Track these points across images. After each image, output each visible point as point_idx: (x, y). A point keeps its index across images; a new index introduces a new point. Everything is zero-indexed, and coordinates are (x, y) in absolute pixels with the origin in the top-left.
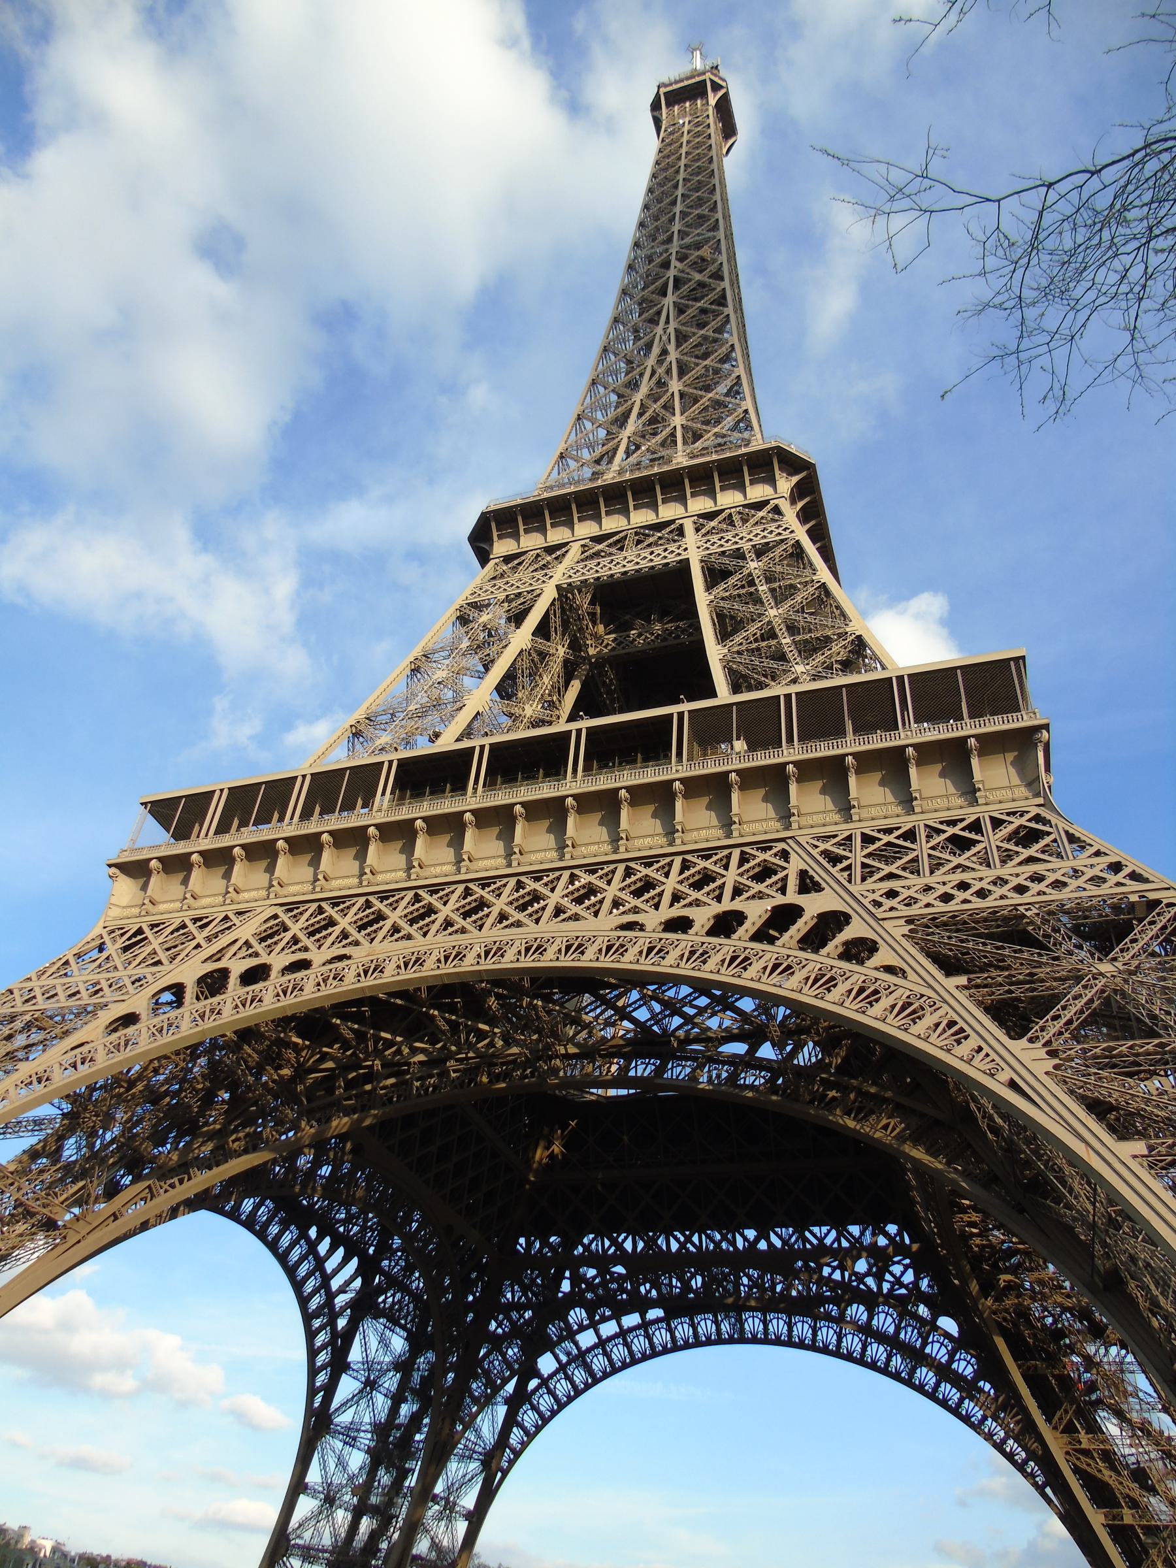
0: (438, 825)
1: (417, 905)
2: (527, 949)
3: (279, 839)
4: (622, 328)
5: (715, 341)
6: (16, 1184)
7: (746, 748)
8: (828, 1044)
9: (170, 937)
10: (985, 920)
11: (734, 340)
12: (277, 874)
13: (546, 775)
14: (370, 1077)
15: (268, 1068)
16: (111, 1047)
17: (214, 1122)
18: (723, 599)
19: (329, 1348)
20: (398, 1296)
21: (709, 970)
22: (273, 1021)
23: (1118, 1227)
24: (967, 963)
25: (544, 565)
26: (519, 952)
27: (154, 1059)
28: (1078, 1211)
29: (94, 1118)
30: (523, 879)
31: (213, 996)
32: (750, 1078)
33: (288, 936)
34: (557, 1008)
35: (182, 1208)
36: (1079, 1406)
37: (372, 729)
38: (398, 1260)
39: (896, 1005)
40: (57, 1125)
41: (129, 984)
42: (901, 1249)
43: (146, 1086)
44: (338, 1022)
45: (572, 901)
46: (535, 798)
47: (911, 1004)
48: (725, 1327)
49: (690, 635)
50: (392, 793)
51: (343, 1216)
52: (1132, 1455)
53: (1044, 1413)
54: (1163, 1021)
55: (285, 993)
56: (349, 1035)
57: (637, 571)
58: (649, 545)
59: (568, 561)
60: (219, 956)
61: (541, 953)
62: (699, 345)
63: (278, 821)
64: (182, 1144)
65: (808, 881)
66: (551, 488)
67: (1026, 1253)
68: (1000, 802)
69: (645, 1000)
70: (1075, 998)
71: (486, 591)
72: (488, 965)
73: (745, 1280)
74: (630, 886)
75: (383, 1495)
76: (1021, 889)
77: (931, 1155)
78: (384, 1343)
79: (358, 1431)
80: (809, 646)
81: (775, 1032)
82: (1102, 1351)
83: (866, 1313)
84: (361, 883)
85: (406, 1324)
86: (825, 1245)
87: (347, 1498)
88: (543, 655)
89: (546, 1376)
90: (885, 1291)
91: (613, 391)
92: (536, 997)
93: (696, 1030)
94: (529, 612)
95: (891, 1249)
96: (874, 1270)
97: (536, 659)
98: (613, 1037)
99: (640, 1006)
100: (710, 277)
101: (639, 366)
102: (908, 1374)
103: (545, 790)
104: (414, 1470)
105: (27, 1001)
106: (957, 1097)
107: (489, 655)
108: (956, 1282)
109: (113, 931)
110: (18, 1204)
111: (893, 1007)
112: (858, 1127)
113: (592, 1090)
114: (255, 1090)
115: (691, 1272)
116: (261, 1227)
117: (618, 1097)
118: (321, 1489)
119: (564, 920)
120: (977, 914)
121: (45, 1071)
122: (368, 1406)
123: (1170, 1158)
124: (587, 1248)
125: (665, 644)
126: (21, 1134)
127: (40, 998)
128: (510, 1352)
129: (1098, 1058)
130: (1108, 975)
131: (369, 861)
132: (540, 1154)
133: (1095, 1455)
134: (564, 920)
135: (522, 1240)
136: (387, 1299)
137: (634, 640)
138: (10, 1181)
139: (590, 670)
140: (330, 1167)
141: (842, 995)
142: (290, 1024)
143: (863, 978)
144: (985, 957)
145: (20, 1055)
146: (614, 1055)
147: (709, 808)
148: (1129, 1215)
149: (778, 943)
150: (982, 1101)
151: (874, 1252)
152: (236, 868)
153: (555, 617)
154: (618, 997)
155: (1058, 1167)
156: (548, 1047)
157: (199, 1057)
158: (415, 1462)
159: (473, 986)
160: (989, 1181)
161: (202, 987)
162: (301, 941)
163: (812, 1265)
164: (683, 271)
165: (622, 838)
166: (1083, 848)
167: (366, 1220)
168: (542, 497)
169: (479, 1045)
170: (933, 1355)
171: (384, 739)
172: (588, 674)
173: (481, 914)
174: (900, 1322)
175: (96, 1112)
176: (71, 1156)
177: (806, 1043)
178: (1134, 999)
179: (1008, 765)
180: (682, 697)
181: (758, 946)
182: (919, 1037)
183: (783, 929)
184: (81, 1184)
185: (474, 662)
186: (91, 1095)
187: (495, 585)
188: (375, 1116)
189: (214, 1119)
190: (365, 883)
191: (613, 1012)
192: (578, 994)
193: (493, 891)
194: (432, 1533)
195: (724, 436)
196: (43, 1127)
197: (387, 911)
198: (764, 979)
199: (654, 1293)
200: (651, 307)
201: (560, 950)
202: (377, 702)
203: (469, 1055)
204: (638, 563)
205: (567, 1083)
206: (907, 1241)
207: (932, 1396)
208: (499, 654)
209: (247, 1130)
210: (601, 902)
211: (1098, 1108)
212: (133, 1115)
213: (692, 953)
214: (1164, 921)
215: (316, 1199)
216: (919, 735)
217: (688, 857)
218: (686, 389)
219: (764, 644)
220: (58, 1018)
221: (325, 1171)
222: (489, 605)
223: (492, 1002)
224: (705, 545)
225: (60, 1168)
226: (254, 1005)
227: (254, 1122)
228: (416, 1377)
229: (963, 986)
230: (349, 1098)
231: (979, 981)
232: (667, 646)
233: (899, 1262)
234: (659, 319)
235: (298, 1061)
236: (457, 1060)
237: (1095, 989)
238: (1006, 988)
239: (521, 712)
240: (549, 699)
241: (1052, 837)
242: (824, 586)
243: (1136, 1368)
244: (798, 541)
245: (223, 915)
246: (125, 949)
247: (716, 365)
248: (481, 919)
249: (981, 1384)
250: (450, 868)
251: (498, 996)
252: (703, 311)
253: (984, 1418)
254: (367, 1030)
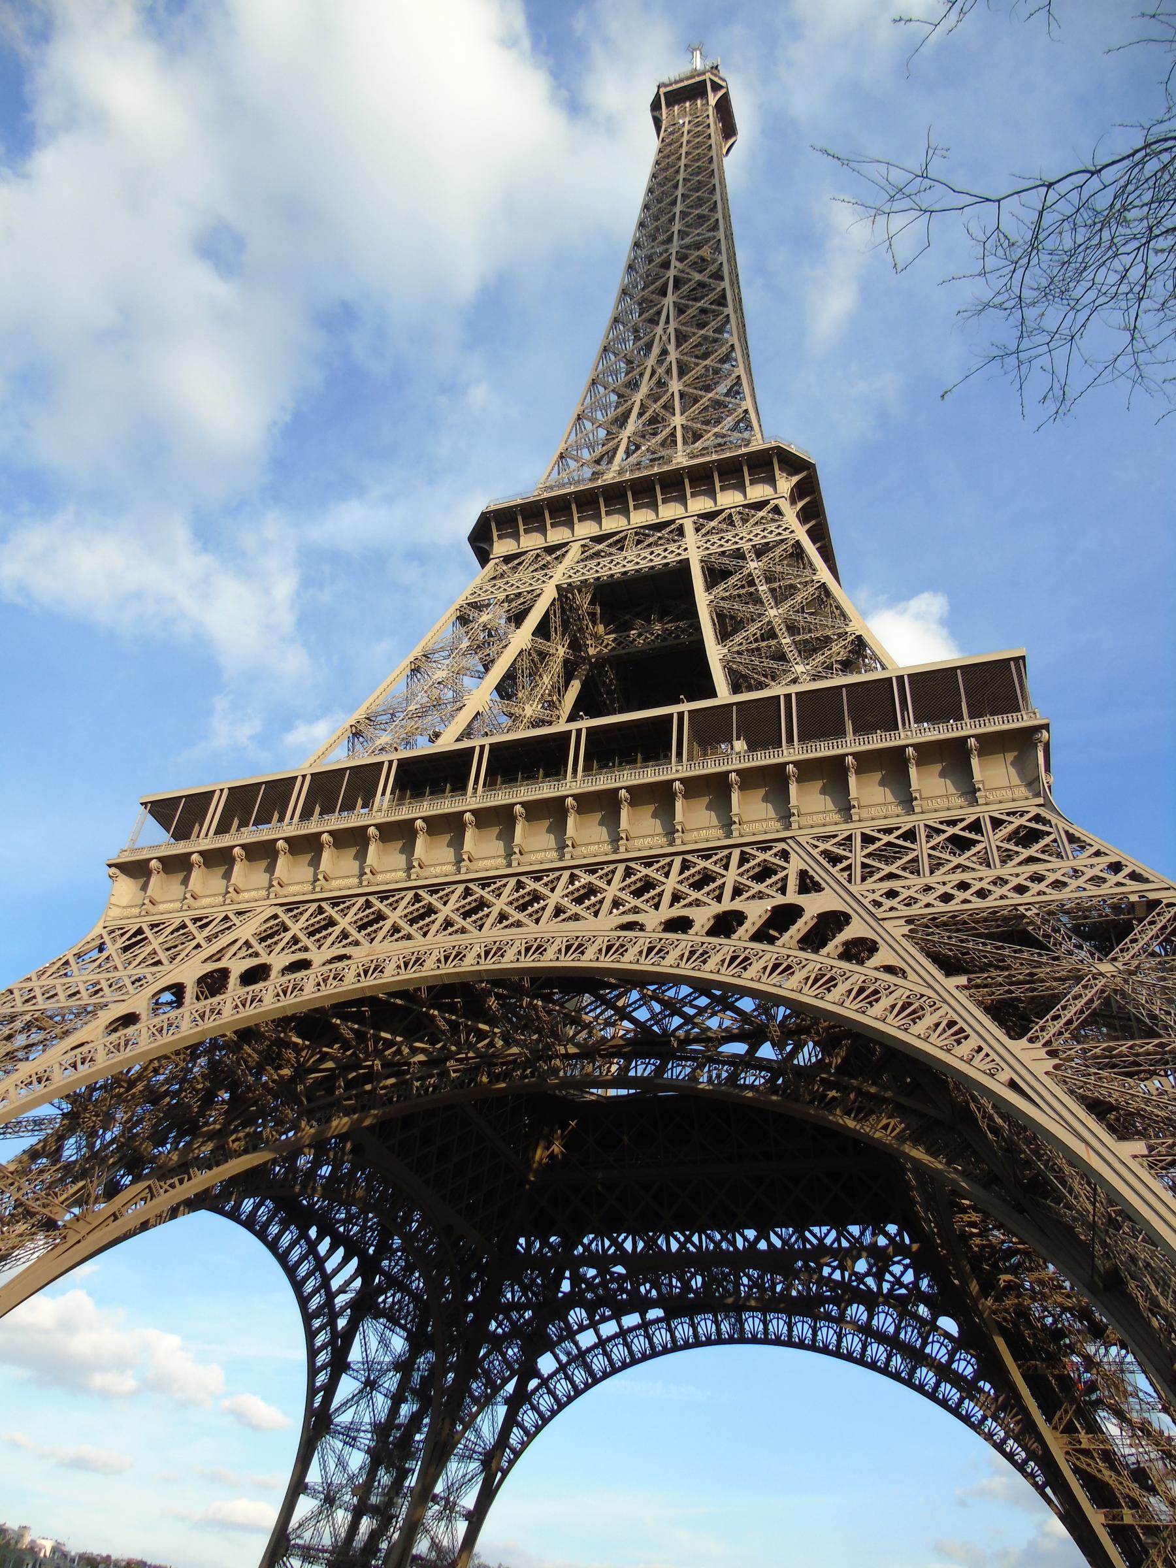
0: (438, 825)
1: (417, 905)
2: (527, 949)
3: (279, 839)
4: (622, 328)
5: (715, 341)
6: (16, 1184)
7: (746, 748)
8: (828, 1044)
9: (170, 937)
10: (985, 920)
11: (734, 340)
12: (277, 874)
13: (546, 775)
14: (370, 1077)
15: (268, 1068)
16: (111, 1047)
17: (214, 1122)
18: (723, 599)
19: (329, 1348)
20: (398, 1296)
21: (709, 970)
22: (273, 1021)
23: (1118, 1227)
24: (967, 963)
25: (544, 565)
26: (519, 952)
27: (154, 1059)
28: (1078, 1211)
29: (94, 1118)
30: (523, 879)
31: (213, 996)
32: (750, 1078)
33: (288, 936)
34: (557, 1008)
35: (182, 1208)
36: (1079, 1406)
37: (372, 729)
38: (398, 1260)
39: (896, 1005)
40: (57, 1125)
41: (129, 984)
42: (901, 1249)
43: (146, 1086)
44: (338, 1022)
45: (572, 901)
46: (535, 798)
47: (911, 1004)
48: (725, 1327)
49: (690, 635)
50: (392, 793)
51: (343, 1216)
52: (1132, 1455)
53: (1044, 1413)
54: (1163, 1021)
55: (285, 993)
56: (349, 1035)
57: (637, 571)
58: (649, 545)
59: (568, 561)
60: (219, 956)
61: (541, 953)
62: (699, 345)
63: (278, 821)
64: (182, 1144)
65: (808, 881)
66: (551, 488)
67: (1026, 1253)
68: (1000, 802)
69: (645, 1000)
70: (1075, 998)
71: (486, 591)
72: (488, 965)
73: (745, 1280)
74: (630, 886)
75: (383, 1495)
76: (1021, 889)
77: (931, 1155)
78: (384, 1343)
79: (358, 1431)
80: (809, 646)
81: (775, 1032)
82: (1102, 1351)
83: (866, 1313)
84: (361, 883)
85: (406, 1324)
86: (825, 1245)
87: (347, 1498)
88: (543, 655)
89: (546, 1376)
90: (885, 1291)
91: (613, 391)
92: (536, 997)
93: (696, 1030)
94: (529, 612)
95: (891, 1249)
96: (874, 1270)
97: (536, 659)
98: (613, 1037)
99: (640, 1006)
100: (710, 277)
101: (639, 366)
102: (908, 1374)
103: (545, 790)
104: (414, 1470)
105: (27, 1001)
106: (957, 1097)
107: (489, 655)
108: (956, 1282)
109: (113, 931)
111: (893, 1007)
112: (858, 1127)
113: (592, 1090)
114: (255, 1090)
115: (691, 1272)
116: (261, 1227)
117: (618, 1097)
118: (321, 1489)
119: (564, 920)
120: (977, 914)
121: (45, 1071)
122: (368, 1406)
123: (1170, 1158)
124: (587, 1248)
125: (665, 644)
126: (21, 1134)
127: (40, 998)
128: (510, 1352)
129: (1098, 1058)
130: (1108, 975)
131: (369, 861)
132: (540, 1154)
133: (1095, 1455)
134: (564, 920)
135: (522, 1240)
136: (387, 1299)
137: (634, 640)
138: (10, 1181)
139: (590, 670)
140: (330, 1167)
141: (842, 995)
142: (290, 1024)
143: (863, 978)
144: (985, 957)
145: (20, 1055)
146: (614, 1055)
147: (709, 808)
148: (1129, 1215)
149: (778, 943)
150: (982, 1101)
151: (874, 1252)
152: (236, 868)
153: (555, 617)
154: (618, 997)
155: (1058, 1167)
156: (548, 1047)
157: (199, 1057)
158: (415, 1462)
159: (473, 986)
160: (989, 1181)
161: (202, 987)
162: (301, 941)
163: (812, 1265)
164: (683, 271)
165: (622, 838)
166: (1083, 848)
167: (366, 1220)
168: (542, 497)
169: (479, 1045)
170: (933, 1355)
171: (384, 739)
172: (588, 674)
173: (481, 914)
174: (900, 1322)
175: (96, 1112)
176: (71, 1156)
177: (806, 1043)
178: (1134, 999)
179: (1008, 765)
180: (682, 697)
181: (758, 946)
182: (919, 1037)
183: (783, 929)
184: (81, 1184)
185: (474, 662)
186: (91, 1095)
187: (495, 585)
188: (375, 1116)
189: (214, 1119)
190: (365, 883)
191: (613, 1012)
192: (578, 994)
193: (493, 891)
194: (432, 1533)
195: (724, 436)
196: (43, 1127)
197: (387, 911)
198: (764, 979)
199: (654, 1293)
200: (651, 307)
201: (560, 950)
202: (377, 702)
203: (469, 1055)
204: (638, 563)
205: (567, 1083)
206: (907, 1241)
207: (932, 1396)
208: (499, 654)
209: (247, 1130)
210: (601, 902)
211: (1098, 1108)
212: (133, 1115)
213: (692, 953)
214: (1164, 921)
215: (316, 1199)
216: (919, 735)
217: (688, 857)
218: (686, 389)
219: (764, 644)
220: (58, 1018)
221: (325, 1171)
222: (489, 605)
223: (492, 1002)
224: (705, 545)
225: (60, 1168)
226: (254, 1005)
227: (254, 1122)
228: (416, 1377)
229: (963, 986)
230: (349, 1098)
231: (979, 981)
232: (667, 646)
233: (899, 1262)
234: (659, 319)
235: (298, 1061)
236: (457, 1060)
237: (1095, 989)
238: (1006, 988)
239: (521, 712)
240: (549, 699)
241: (1052, 837)
242: (824, 586)
244: (798, 541)
245: (223, 915)
246: (125, 949)
247: (716, 365)
248: (481, 919)
249: (981, 1384)
250: (450, 868)
251: (498, 996)
252: (703, 311)
253: (984, 1418)
254: (367, 1030)
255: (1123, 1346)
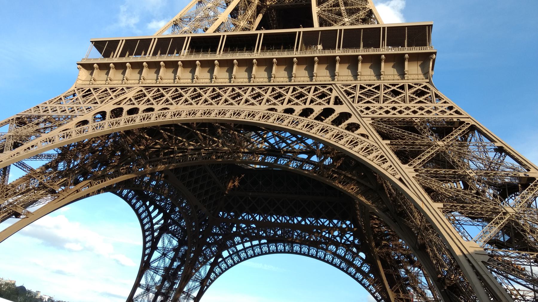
1: (195, 93)
3: (144, 62)
6: (40, 177)
7: (322, 48)
8: (335, 159)
9: (101, 94)
10: (400, 121)
13: (247, 50)
14: (173, 152)
15: (136, 145)
16: (78, 131)
17: (115, 162)
20: (176, 227)
21: (298, 129)
22: (138, 129)
23: (428, 230)
24: (391, 136)
26: (231, 114)
28: (415, 224)
29: (71, 156)
31: (117, 117)
32: (307, 167)
33: (146, 98)
35: (102, 191)
36: (401, 285)
37: (182, 24)
38: (177, 215)
41: (85, 110)
42: (350, 229)
43: (90, 147)
44: (163, 132)
45: (252, 98)
47: (369, 148)
50: (188, 49)
51: (159, 199)
53: (389, 286)
56: (166, 137)
60: (119, 103)
61: (239, 116)
63: (144, 55)
64: (102, 169)
65: (338, 100)
67: (393, 235)
68: (413, 79)
69: (274, 136)
70: (427, 152)
72: (219, 117)
74: (273, 95)
75: (166, 290)
76: (415, 112)
77: (367, 200)
78: (171, 242)
81: (319, 153)
82: (412, 269)
84: (174, 82)
85: (178, 236)
86: (324, 225)
87: (154, 290)
90: (343, 242)
92: (236, 131)
93: (290, 148)
95: (347, 229)
96: (340, 235)
97: (247, 3)
98: (261, 148)
99: (272, 138)
102: (347, 269)
103: (246, 56)
104: (177, 283)
105: (45, 111)
108: (367, 242)
109: (79, 89)
110: (41, 184)
111: (362, 148)
112: (343, 188)
113: (251, 165)
115: (278, 229)
116: (129, 200)
119: (248, 105)
120: (398, 119)
122: (163, 262)
123: (451, 210)
125: (296, 4)
126: (43, 159)
128: (213, 249)
129: (432, 174)
130: (441, 146)
131: (178, 74)
132: (230, 185)
133: (404, 300)
134: (248, 105)
138: (38, 175)
141: (345, 142)
143: (353, 137)
144: (398, 135)
145: (42, 131)
146: (260, 154)
148: (433, 226)
149: (324, 121)
150: (388, 184)
151: (341, 229)
152: (127, 71)
154: (265, 134)
155: (411, 208)
156: (238, 149)
157: (110, 139)
160: (385, 211)
161: (113, 114)
163: (319, 231)
165: (252, 78)
166: (440, 100)
169: (213, 145)
171: (186, 28)
172: (266, 12)
173: (218, 99)
174: (346, 252)
176: (62, 169)
177: (327, 158)
178: (448, 155)
181: (317, 122)
182: (370, 160)
183: (327, 116)
184: (65, 179)
186: (69, 148)
189: (115, 161)
190: (176, 82)
193: (223, 91)
197: (183, 94)
201: (246, 115)
202: (185, 13)
203: (210, 148)
205: (243, 162)
206: (353, 227)
207: (353, 277)
209: (127, 166)
210: (262, 100)
211: (428, 190)
212: (85, 157)
213: (293, 122)
214: (465, 129)
215: (149, 192)
216: (414, 50)
217: (296, 87)
219: (334, 8)
220: (57, 119)
221: (154, 183)
223: (220, 130)
225: (57, 173)
226: (132, 122)
227: (130, 164)
228: (180, 254)
229: (388, 144)
230: (165, 159)
231: (394, 143)
233: (349, 234)
235: (147, 144)
236: (205, 150)
237: (435, 150)
238: (404, 146)
239: (239, 24)
240: (250, 20)
241: (429, 95)
243: (422, 275)
246: (84, 96)
248: (218, 101)
249: (370, 275)
251: (222, 129)
253: (370, 285)
254: (173, 136)
255: (420, 267)
